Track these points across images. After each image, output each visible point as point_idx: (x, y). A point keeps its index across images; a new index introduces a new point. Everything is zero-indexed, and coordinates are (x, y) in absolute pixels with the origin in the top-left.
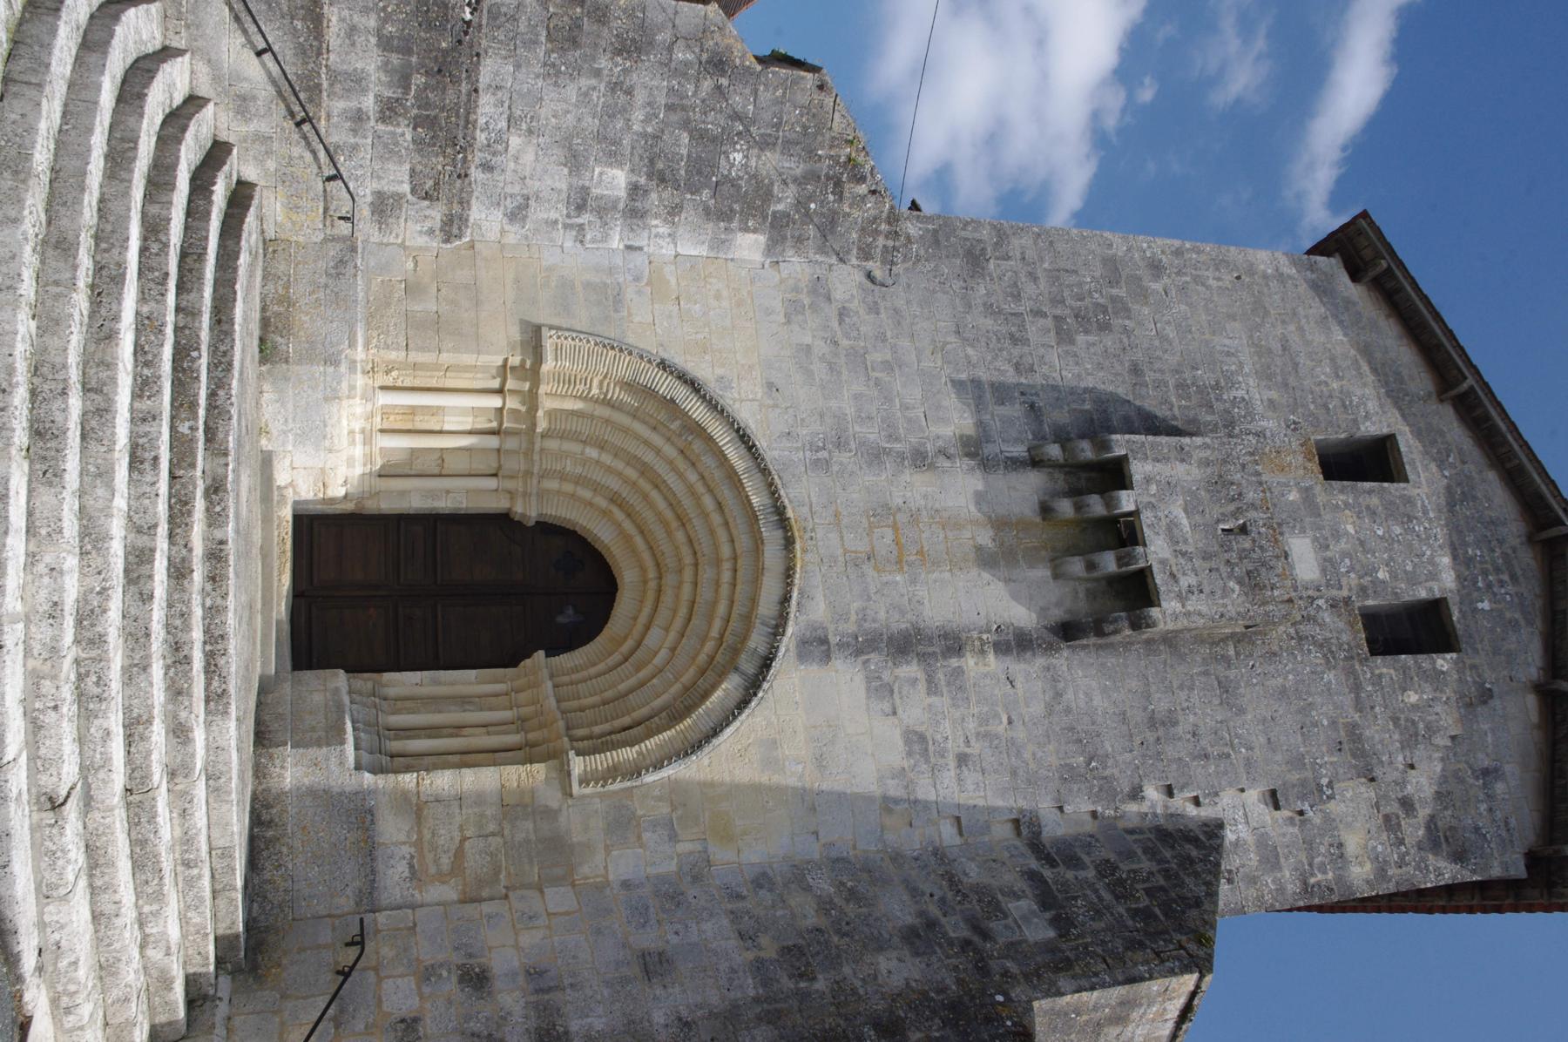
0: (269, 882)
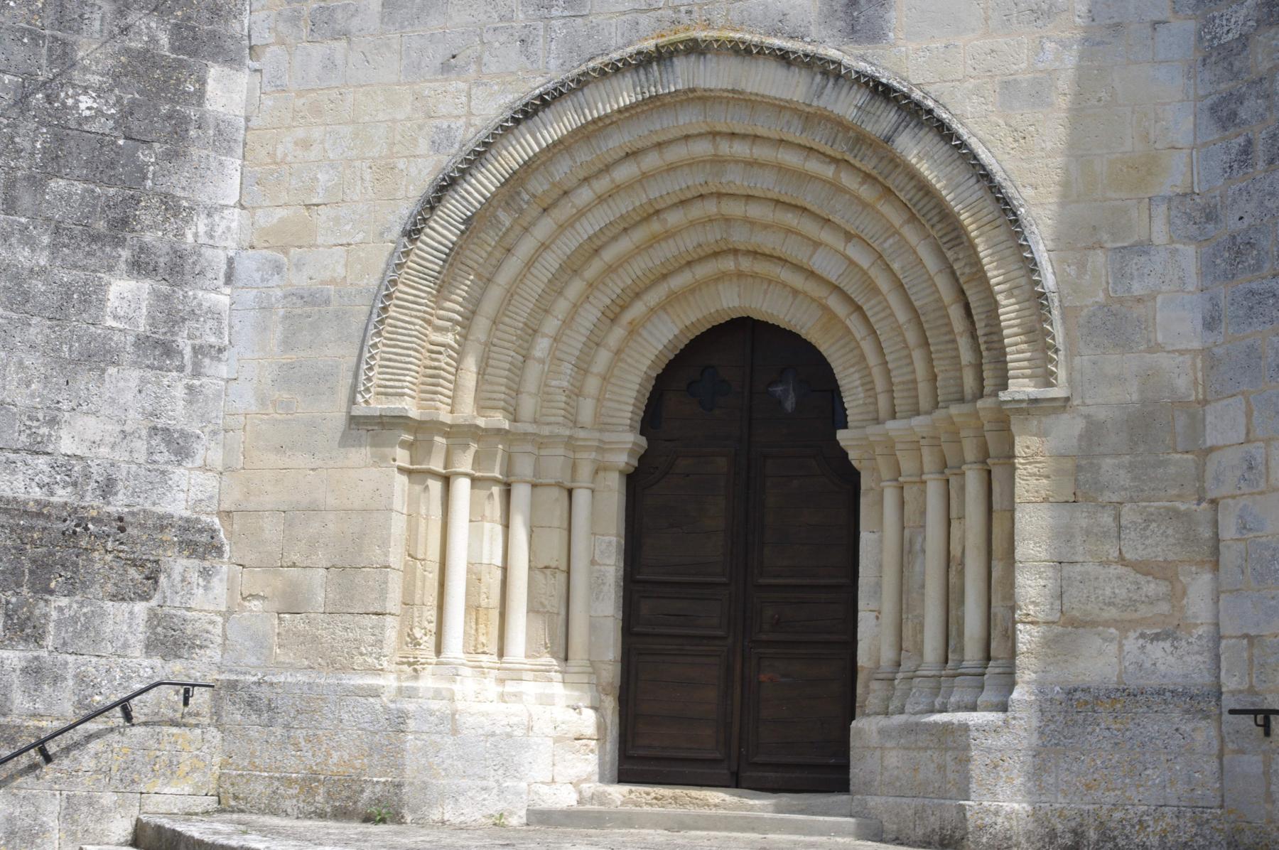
0: (1163, 838)
